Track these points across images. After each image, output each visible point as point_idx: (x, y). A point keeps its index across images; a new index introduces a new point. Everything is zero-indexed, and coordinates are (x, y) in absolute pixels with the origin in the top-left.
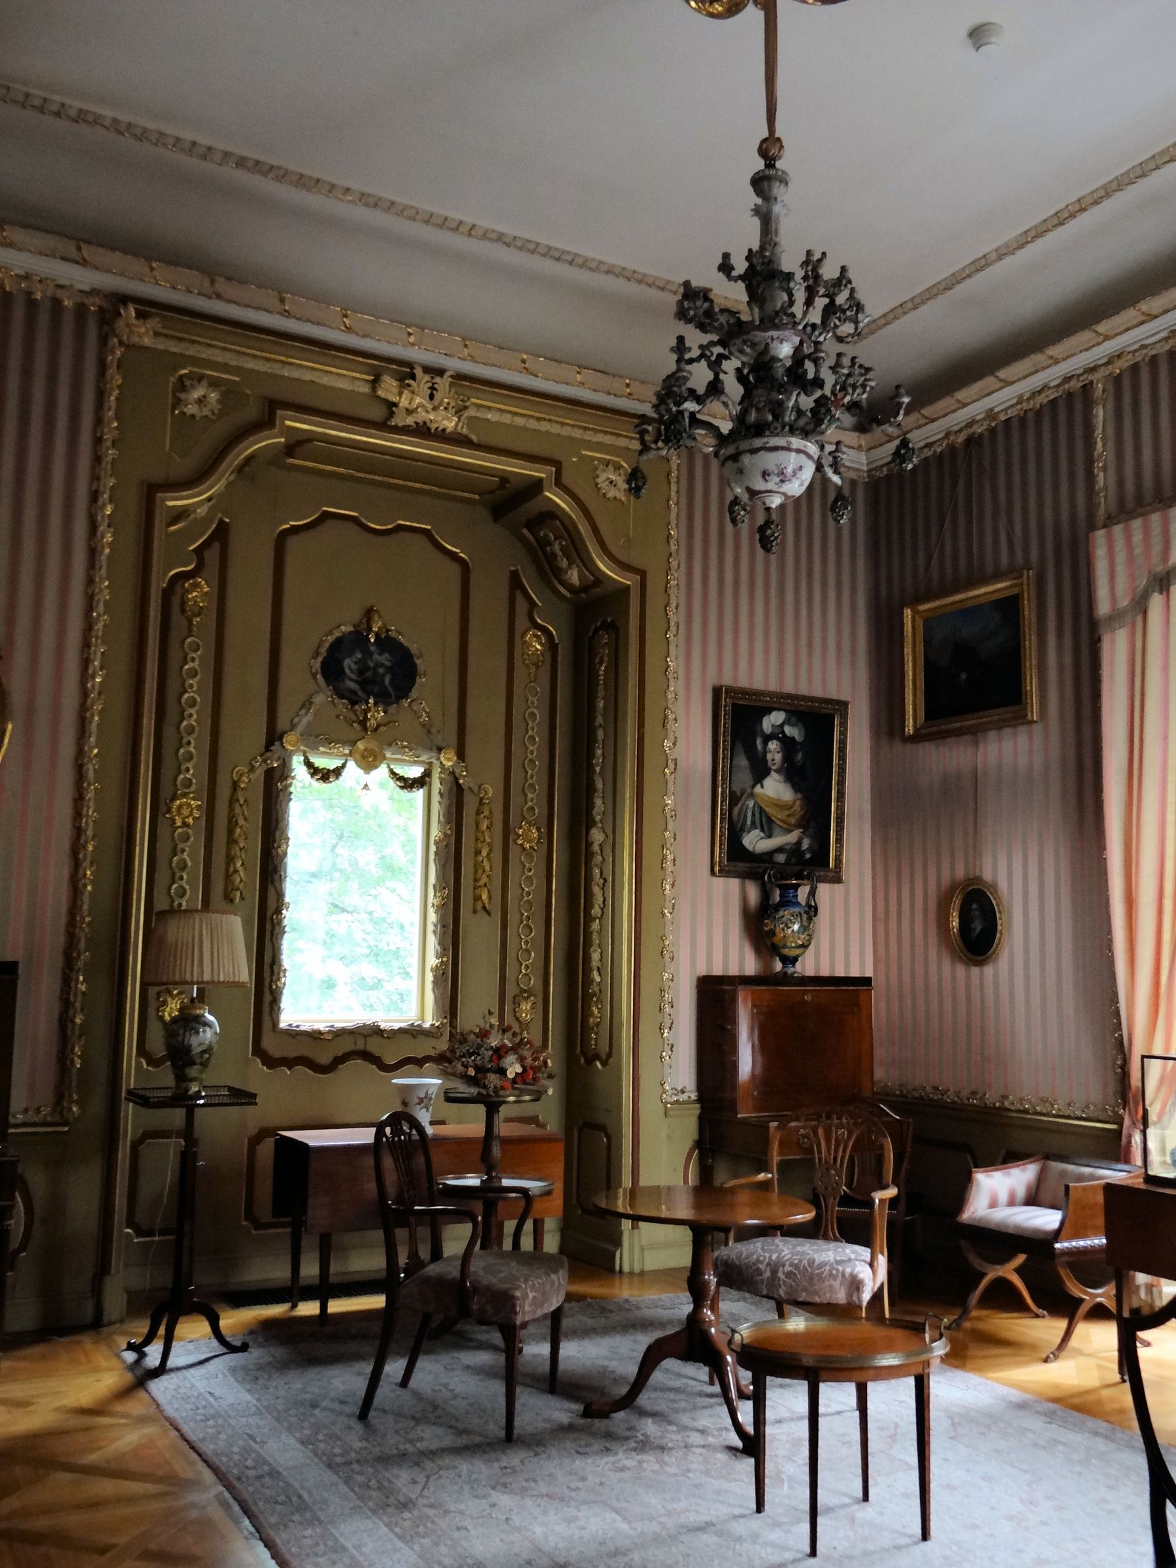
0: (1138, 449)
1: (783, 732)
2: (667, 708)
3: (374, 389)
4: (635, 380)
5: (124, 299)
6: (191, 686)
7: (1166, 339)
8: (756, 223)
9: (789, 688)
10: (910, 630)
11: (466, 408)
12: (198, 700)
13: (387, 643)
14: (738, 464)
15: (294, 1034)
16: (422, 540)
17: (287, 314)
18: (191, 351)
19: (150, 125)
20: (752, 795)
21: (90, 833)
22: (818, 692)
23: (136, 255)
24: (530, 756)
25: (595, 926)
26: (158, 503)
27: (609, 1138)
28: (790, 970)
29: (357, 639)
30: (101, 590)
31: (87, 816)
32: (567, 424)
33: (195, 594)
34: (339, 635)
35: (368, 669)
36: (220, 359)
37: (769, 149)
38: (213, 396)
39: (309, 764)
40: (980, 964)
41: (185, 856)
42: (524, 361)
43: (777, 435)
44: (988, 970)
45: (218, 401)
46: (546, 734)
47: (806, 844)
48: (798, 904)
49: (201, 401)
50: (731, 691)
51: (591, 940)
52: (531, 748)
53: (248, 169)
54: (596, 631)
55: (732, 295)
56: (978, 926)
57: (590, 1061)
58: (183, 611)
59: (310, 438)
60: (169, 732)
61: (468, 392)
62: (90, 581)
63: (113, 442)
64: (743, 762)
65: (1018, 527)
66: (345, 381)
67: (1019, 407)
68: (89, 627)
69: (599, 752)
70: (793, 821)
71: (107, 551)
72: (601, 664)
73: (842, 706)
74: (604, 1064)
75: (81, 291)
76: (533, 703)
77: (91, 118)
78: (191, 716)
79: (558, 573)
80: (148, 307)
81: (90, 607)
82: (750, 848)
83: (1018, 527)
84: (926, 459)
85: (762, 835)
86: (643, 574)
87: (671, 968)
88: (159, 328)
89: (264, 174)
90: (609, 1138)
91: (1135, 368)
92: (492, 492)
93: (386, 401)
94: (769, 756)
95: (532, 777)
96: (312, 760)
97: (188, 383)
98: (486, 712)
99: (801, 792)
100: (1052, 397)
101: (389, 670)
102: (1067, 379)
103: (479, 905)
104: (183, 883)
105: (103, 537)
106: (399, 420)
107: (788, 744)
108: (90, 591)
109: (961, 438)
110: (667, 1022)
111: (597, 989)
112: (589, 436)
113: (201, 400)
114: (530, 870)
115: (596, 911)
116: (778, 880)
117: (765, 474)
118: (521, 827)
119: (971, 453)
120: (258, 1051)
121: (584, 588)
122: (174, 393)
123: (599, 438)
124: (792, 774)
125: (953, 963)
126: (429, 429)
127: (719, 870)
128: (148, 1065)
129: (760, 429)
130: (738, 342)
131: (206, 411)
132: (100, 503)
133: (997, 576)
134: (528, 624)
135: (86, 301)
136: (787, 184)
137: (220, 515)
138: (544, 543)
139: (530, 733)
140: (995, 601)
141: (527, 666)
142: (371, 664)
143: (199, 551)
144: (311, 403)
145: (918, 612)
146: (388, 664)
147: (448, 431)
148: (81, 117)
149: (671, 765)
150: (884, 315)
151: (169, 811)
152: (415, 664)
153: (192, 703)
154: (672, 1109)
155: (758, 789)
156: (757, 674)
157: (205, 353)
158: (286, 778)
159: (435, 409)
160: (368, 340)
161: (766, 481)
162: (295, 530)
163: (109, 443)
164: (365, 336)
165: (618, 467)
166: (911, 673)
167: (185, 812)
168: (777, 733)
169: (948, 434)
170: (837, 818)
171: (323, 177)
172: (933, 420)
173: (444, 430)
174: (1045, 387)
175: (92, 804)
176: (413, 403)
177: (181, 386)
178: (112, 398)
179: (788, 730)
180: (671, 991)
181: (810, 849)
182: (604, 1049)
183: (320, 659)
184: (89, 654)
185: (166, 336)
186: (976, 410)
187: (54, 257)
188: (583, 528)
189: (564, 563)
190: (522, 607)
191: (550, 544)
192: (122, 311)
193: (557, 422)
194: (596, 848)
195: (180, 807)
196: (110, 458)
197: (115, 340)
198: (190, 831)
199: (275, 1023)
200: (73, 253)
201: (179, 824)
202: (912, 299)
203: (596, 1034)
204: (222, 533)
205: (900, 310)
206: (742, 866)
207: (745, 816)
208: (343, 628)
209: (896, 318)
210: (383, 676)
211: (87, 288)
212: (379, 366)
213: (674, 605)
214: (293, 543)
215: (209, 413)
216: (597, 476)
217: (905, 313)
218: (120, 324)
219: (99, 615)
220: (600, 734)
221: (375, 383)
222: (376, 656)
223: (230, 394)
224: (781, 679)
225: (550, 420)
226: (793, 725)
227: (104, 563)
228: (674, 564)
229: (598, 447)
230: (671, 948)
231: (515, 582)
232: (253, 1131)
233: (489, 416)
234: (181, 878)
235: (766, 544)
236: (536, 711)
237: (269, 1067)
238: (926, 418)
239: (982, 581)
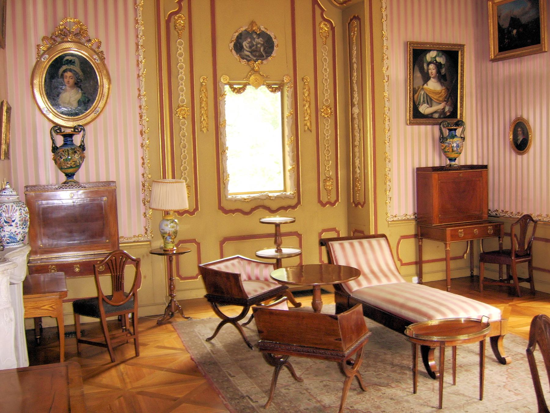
1: (436, 60)
6: (181, 61)
9: (438, 40)
10: (491, 12)
13: (263, 35)
20: (423, 89)
35: (253, 46)
39: (231, 86)
40: (518, 153)
46: (332, 67)
47: (447, 109)
50: (411, 43)
57: (356, 205)
64: (418, 75)
70: (441, 99)
71: (141, 9)
74: (362, 206)
85: (428, 106)
87: (389, 165)
94: (430, 71)
101: (262, 45)
103: (306, 127)
107: (439, 66)
115: (357, 143)
118: (323, 108)
124: (441, 78)
134: (321, 20)
139: (325, 67)
140: (59, 355)
141: (322, 38)
142: (255, 43)
144: (317, 191)
145: (494, 3)
146: (262, 42)
155: (425, 86)
156: (424, 35)
166: (492, 31)
170: (461, 96)
180: (389, 175)
182: (362, 201)
190: (318, 11)
206: (419, 120)
207: (420, 99)
210: (260, 48)
213: (384, 7)
226: (441, 57)
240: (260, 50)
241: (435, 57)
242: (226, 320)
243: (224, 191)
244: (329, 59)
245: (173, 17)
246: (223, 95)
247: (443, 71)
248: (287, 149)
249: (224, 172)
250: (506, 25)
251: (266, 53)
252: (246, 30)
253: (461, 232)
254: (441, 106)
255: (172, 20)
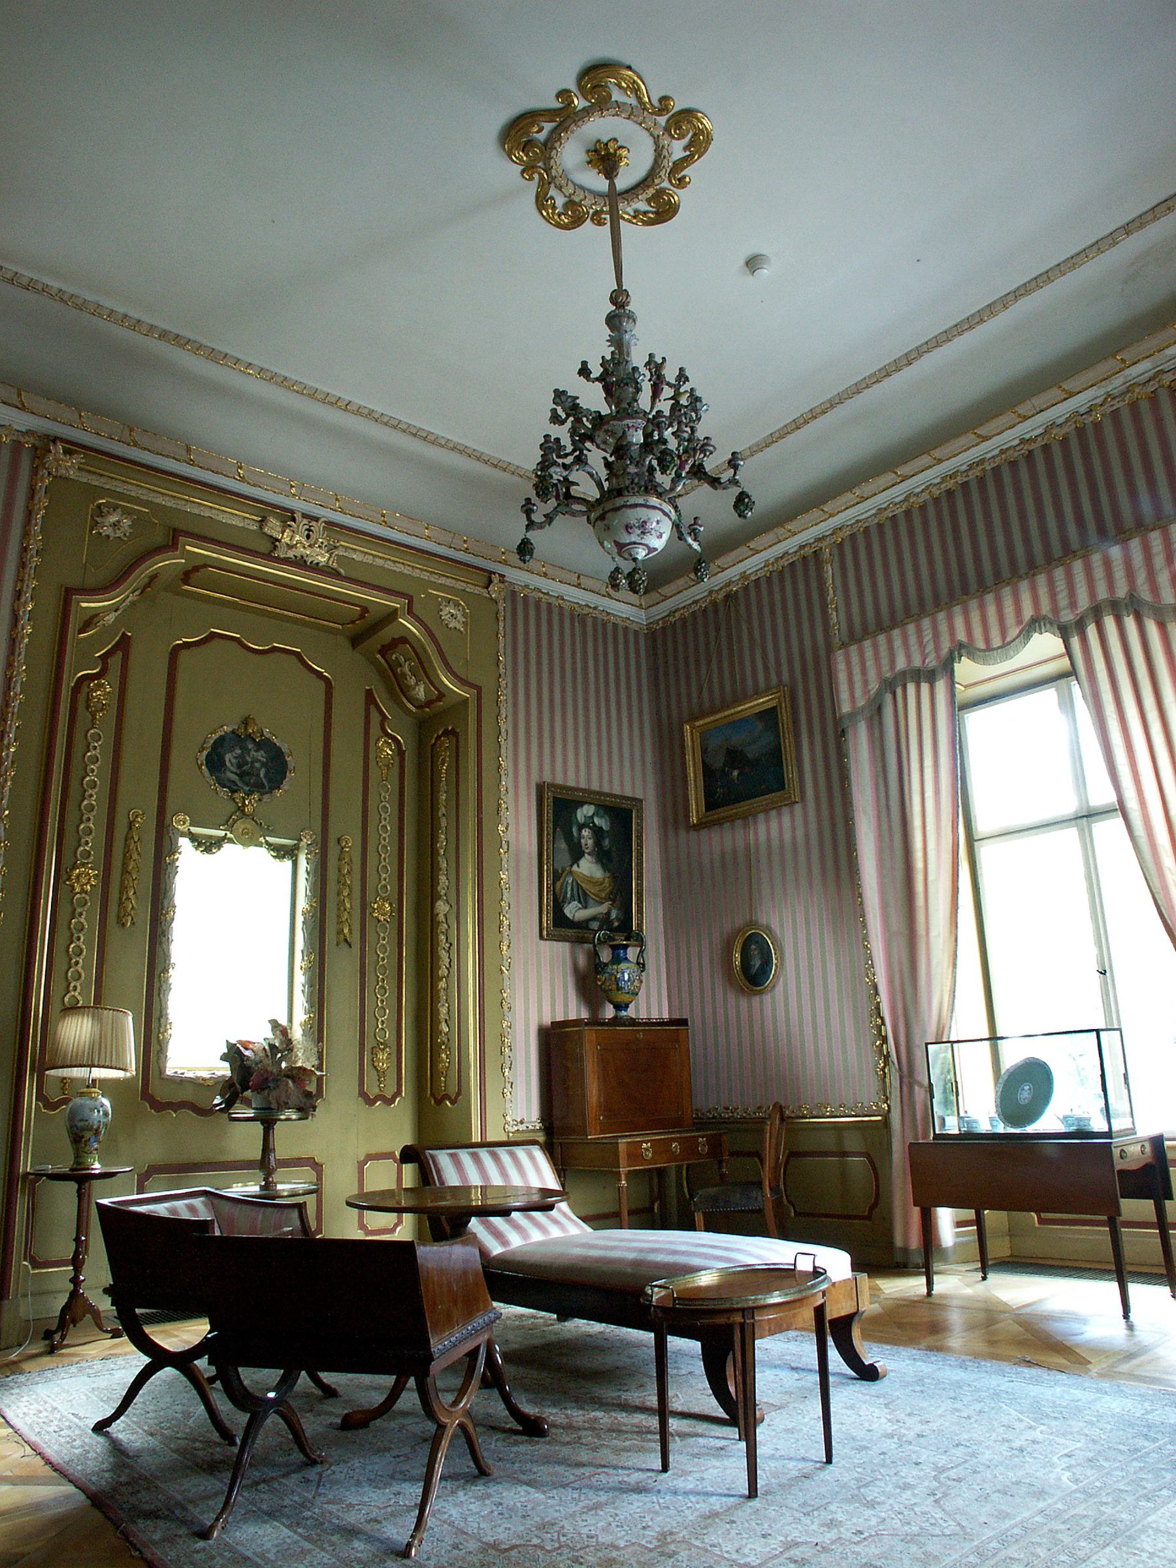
0: (861, 592)
3: (261, 528)
5: (55, 440)
7: (875, 515)
9: (595, 786)
11: (336, 547)
13: (265, 744)
14: (606, 522)
15: (181, 1082)
17: (191, 463)
19: (90, 297)
23: (69, 405)
26: (74, 604)
29: (237, 739)
30: (19, 674)
36: (133, 494)
37: (619, 298)
38: (126, 522)
44: (767, 998)
49: (115, 525)
50: (552, 786)
53: (169, 342)
54: (438, 738)
55: (593, 398)
56: (757, 963)
57: (439, 1102)
58: (88, 707)
60: (71, 806)
61: (338, 537)
64: (563, 845)
65: (771, 657)
77: (40, 287)
78: (91, 796)
79: (405, 690)
80: (72, 448)
83: (771, 657)
86: (479, 690)
87: (509, 1016)
89: (182, 346)
91: (853, 536)
92: (353, 622)
97: (105, 510)
101: (264, 765)
102: (802, 547)
104: (81, 943)
106: (281, 553)
107: (598, 832)
109: (721, 596)
113: (116, 525)
115: (443, 971)
116: (597, 939)
117: (628, 528)
119: (729, 601)
121: (429, 703)
123: (442, 581)
124: (602, 857)
129: (619, 493)
130: (602, 434)
131: (119, 534)
133: (757, 693)
135: (22, 440)
136: (634, 321)
142: (249, 760)
143: (104, 658)
151: (69, 879)
153: (93, 785)
155: (575, 868)
156: (572, 774)
158: (173, 854)
165: (457, 605)
168: (588, 823)
169: (711, 592)
170: (637, 893)
171: (230, 352)
174: (786, 553)
176: (293, 539)
181: (617, 918)
182: (453, 1090)
183: (205, 753)
186: (733, 573)
188: (431, 649)
189: (413, 681)
190: (375, 718)
194: (441, 918)
195: (79, 876)
199: (161, 1071)
200: (14, 399)
201: (78, 890)
204: (124, 644)
207: (566, 893)
212: (265, 510)
214: (184, 655)
219: (16, 694)
220: (444, 822)
221: (263, 522)
223: (140, 522)
224: (589, 780)
229: (441, 588)
239: (746, 698)
240: (258, 775)
241: (592, 817)
242: (160, 1358)
243: (158, 1059)
244: (391, 808)
245: (86, 683)
246: (174, 850)
247: (607, 842)
248: (300, 978)
249: (161, 1016)
250: (718, 762)
251: (269, 781)
252: (233, 732)
253: (646, 1149)
254: (603, 909)
255: (85, 689)
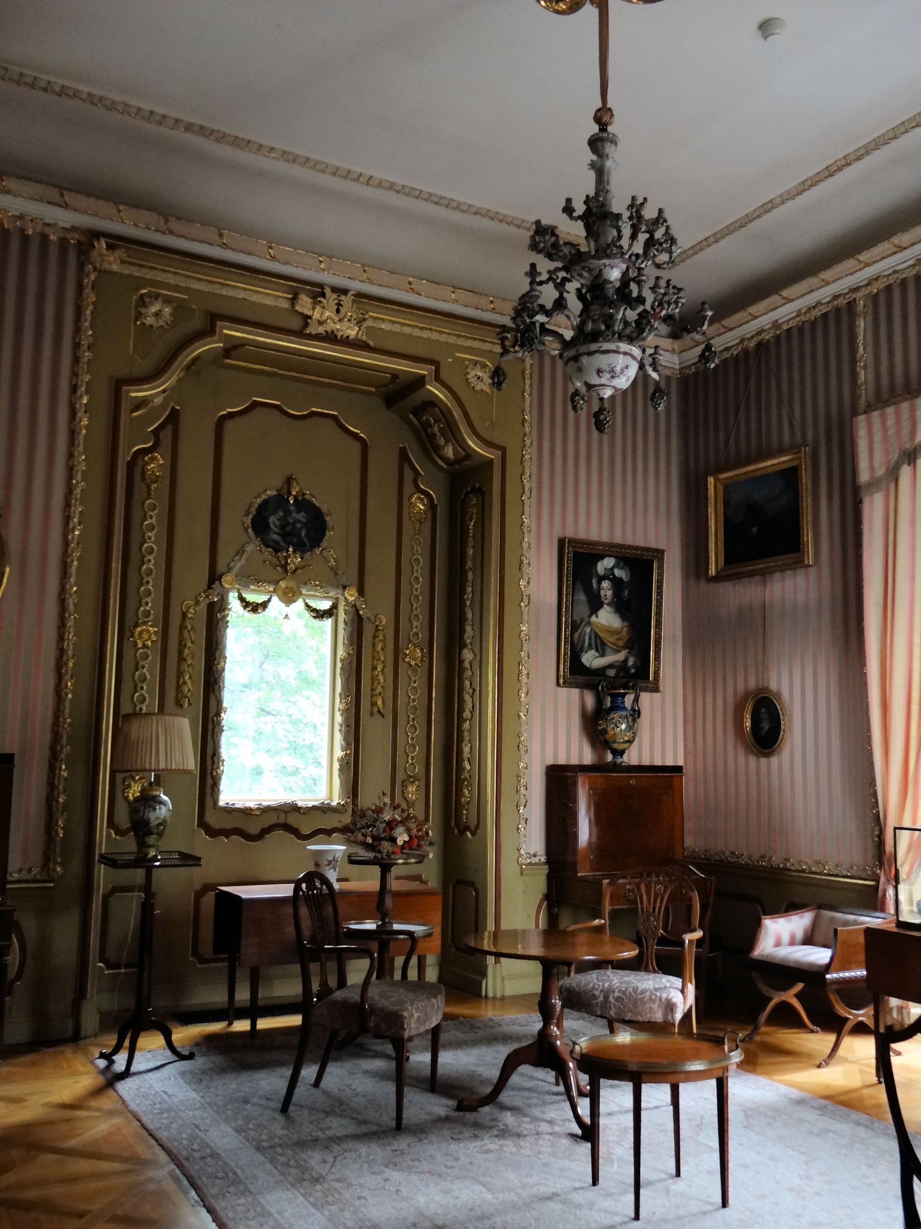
0: (891, 352)
1: (613, 574)
2: (522, 555)
3: (293, 305)
4: (498, 298)
5: (97, 234)
6: (150, 538)
7: (913, 266)
8: (592, 175)
9: (618, 540)
10: (713, 493)
11: (365, 320)
12: (155, 548)
13: (303, 504)
14: (578, 364)
15: (230, 811)
16: (331, 423)
17: (225, 246)
18: (150, 275)
19: (118, 98)
20: (589, 623)
21: (70, 653)
22: (640, 542)
24: (415, 593)
25: (466, 725)
26: (124, 394)
27: (477, 892)
28: (619, 760)
29: (280, 501)
30: (79, 462)
31: (68, 639)
32: (444, 333)
33: (152, 465)
34: (266, 497)
35: (288, 524)
36: (172, 282)
37: (603, 117)
38: (167, 310)
39: (242, 599)
40: (768, 755)
41: (145, 671)
42: (410, 283)
43: (609, 341)
44: (774, 760)
45: (171, 315)
46: (428, 575)
47: (631, 662)
48: (625, 708)
49: (157, 314)
50: (572, 541)
51: (463, 737)
52: (416, 586)
53: (195, 133)
54: (467, 495)
56: (766, 726)
57: (462, 832)
58: (143, 479)
59: (243, 343)
60: (132, 574)
61: (366, 308)
62: (71, 456)
63: (89, 346)
64: (582, 597)
65: (797, 413)
66: (270, 298)
67: (798, 319)
68: (69, 491)
69: (469, 589)
70: (621, 643)
71: (84, 432)
72: (471, 520)
73: (659, 554)
74: (473, 834)
75: (64, 228)
76: (417, 551)
77: (71, 93)
78: (149, 561)
79: (437, 449)
80: (116, 241)
81: (70, 476)
82: (587, 665)
83: (797, 413)
84: (725, 360)
85: (597, 654)
86: (503, 450)
87: (525, 758)
88: (124, 257)
89: (207, 136)
90: (477, 892)
91: (889, 288)
92: (385, 386)
93: (302, 314)
94: (602, 593)
95: (416, 609)
96: (244, 595)
97: (147, 300)
98: (381, 558)
99: (628, 621)
100: (824, 311)
101: (305, 525)
102: (836, 297)
103: (375, 709)
104: (144, 692)
105: (80, 421)
106: (313, 329)
107: (617, 583)
108: (70, 463)
109: (753, 344)
110: (523, 801)
111: (467, 775)
112: (461, 342)
113: (157, 313)
114: (415, 682)
115: (467, 714)
117: (599, 372)
118: (408, 648)
119: (761, 355)
120: (202, 824)
121: (458, 461)
122: (136, 308)
123: (469, 343)
124: (620, 607)
125: (746, 755)
126: (336, 336)
127: (563, 682)
128: (116, 834)
129: (595, 337)
130: (578, 268)
131: (161, 323)
132: (78, 394)
133: (781, 451)
134: (414, 489)
135: (67, 236)
137: (172, 404)
138: (426, 426)
139: (415, 574)
141: (413, 522)
142: (291, 521)
143: (156, 432)
145: (719, 480)
146: (304, 520)
147: (351, 337)
148: (63, 92)
149: (526, 600)
150: (693, 247)
151: (132, 636)
152: (325, 521)
153: (151, 551)
154: (526, 869)
155: (593, 618)
156: (593, 528)
157: (161, 277)
158: (224, 610)
159: (340, 320)
160: (288, 266)
161: (600, 377)
162: (231, 415)
163: (85, 348)
164: (286, 263)
165: (484, 366)
166: (713, 528)
167: (145, 636)
168: (609, 575)
169: (742, 340)
170: (656, 641)
171: (253, 139)
172: (731, 329)
173: (348, 337)
174: (819, 303)
175: (72, 630)
176: (324, 316)
177: (142, 302)
178: (88, 312)
179: (617, 572)
180: (526, 777)
181: (634, 666)
182: (473, 822)
183: (251, 517)
184: (70, 512)
185: (130, 263)
186: (765, 321)
187: (42, 201)
188: (457, 414)
189: (442, 441)
190: (409, 475)
191: (431, 426)
192: (96, 244)
193: (436, 331)
194: (467, 665)
195: (141, 633)
196: (86, 359)
197: (90, 267)
198: (149, 652)
199: (215, 801)
200: (57, 199)
201: (140, 645)
202: (714, 235)
203: (467, 810)
204: (174, 418)
205: (705, 243)
206: (581, 679)
207: (584, 640)
208: (268, 492)
209: (701, 249)
210: (300, 530)
211: (68, 226)
212: (297, 287)
213: (527, 475)
214: (230, 425)
215: (164, 324)
216: (468, 373)
217: (709, 245)
218: (94, 254)
219: (77, 482)
220: (470, 575)
221: (294, 300)
222: (294, 515)
223: (180, 309)
224: (612, 532)
225: (431, 329)
226: (621, 569)
227: (82, 442)
228: (528, 442)
229: (469, 350)
230: (525, 743)
231: (404, 456)
232: (198, 887)
233: (383, 326)
234: (142, 688)
235: (600, 426)
236: (420, 558)
237: (211, 837)
238: (726, 327)
239: (769, 455)
